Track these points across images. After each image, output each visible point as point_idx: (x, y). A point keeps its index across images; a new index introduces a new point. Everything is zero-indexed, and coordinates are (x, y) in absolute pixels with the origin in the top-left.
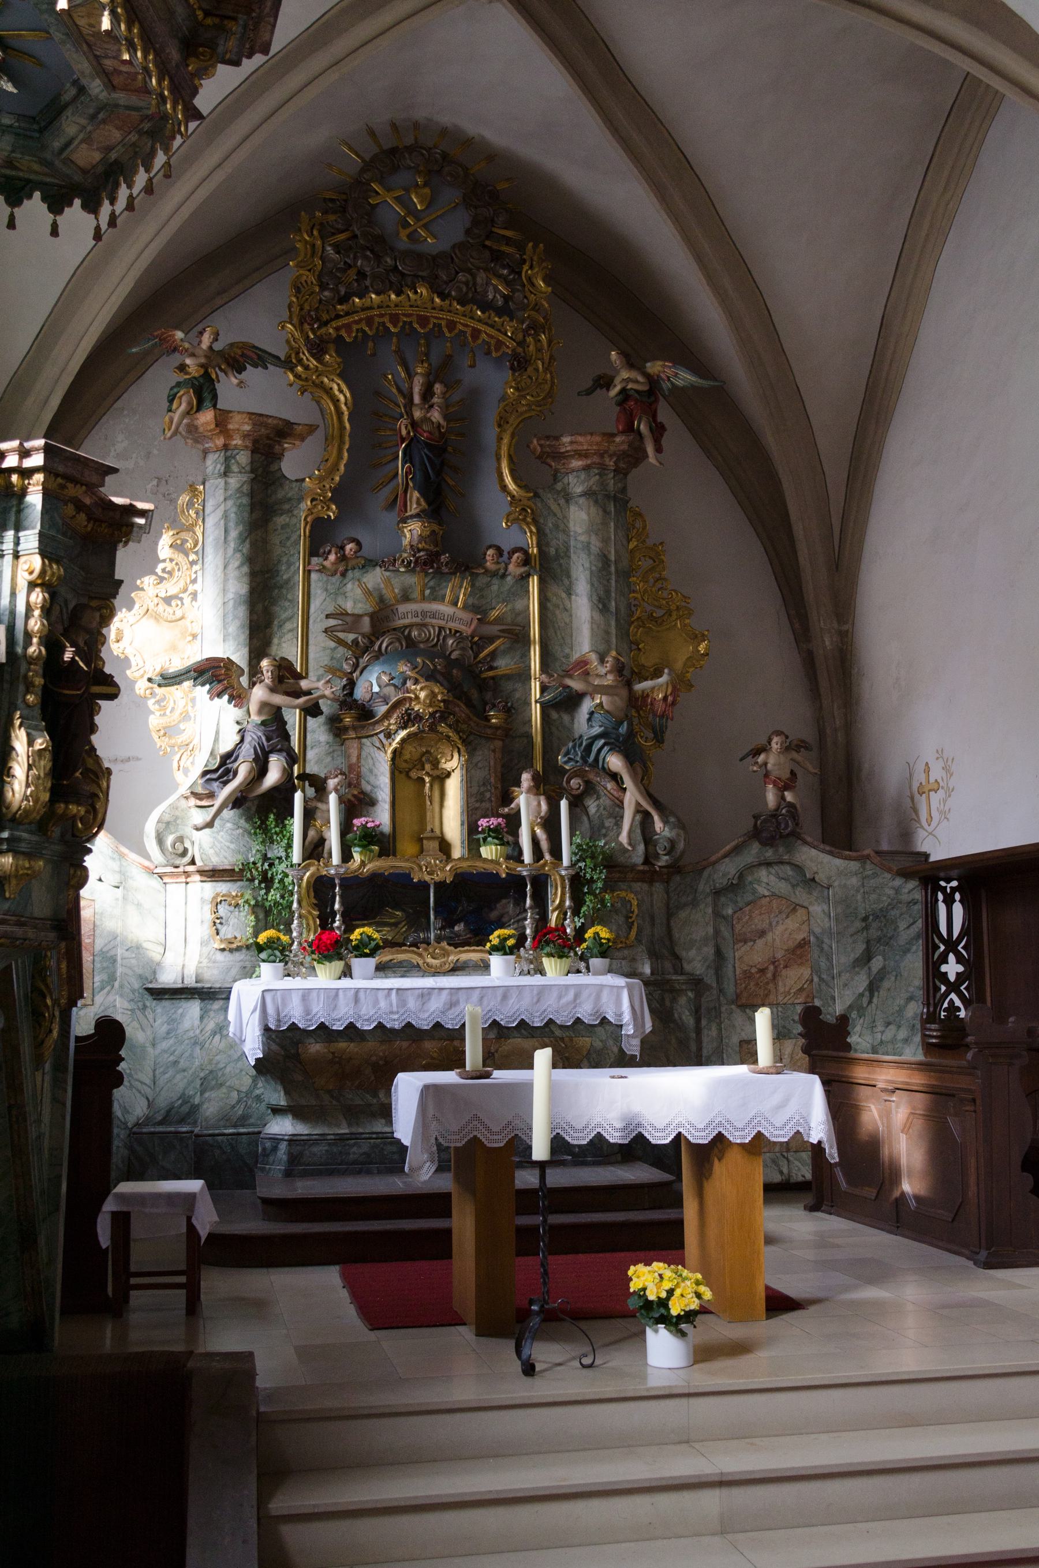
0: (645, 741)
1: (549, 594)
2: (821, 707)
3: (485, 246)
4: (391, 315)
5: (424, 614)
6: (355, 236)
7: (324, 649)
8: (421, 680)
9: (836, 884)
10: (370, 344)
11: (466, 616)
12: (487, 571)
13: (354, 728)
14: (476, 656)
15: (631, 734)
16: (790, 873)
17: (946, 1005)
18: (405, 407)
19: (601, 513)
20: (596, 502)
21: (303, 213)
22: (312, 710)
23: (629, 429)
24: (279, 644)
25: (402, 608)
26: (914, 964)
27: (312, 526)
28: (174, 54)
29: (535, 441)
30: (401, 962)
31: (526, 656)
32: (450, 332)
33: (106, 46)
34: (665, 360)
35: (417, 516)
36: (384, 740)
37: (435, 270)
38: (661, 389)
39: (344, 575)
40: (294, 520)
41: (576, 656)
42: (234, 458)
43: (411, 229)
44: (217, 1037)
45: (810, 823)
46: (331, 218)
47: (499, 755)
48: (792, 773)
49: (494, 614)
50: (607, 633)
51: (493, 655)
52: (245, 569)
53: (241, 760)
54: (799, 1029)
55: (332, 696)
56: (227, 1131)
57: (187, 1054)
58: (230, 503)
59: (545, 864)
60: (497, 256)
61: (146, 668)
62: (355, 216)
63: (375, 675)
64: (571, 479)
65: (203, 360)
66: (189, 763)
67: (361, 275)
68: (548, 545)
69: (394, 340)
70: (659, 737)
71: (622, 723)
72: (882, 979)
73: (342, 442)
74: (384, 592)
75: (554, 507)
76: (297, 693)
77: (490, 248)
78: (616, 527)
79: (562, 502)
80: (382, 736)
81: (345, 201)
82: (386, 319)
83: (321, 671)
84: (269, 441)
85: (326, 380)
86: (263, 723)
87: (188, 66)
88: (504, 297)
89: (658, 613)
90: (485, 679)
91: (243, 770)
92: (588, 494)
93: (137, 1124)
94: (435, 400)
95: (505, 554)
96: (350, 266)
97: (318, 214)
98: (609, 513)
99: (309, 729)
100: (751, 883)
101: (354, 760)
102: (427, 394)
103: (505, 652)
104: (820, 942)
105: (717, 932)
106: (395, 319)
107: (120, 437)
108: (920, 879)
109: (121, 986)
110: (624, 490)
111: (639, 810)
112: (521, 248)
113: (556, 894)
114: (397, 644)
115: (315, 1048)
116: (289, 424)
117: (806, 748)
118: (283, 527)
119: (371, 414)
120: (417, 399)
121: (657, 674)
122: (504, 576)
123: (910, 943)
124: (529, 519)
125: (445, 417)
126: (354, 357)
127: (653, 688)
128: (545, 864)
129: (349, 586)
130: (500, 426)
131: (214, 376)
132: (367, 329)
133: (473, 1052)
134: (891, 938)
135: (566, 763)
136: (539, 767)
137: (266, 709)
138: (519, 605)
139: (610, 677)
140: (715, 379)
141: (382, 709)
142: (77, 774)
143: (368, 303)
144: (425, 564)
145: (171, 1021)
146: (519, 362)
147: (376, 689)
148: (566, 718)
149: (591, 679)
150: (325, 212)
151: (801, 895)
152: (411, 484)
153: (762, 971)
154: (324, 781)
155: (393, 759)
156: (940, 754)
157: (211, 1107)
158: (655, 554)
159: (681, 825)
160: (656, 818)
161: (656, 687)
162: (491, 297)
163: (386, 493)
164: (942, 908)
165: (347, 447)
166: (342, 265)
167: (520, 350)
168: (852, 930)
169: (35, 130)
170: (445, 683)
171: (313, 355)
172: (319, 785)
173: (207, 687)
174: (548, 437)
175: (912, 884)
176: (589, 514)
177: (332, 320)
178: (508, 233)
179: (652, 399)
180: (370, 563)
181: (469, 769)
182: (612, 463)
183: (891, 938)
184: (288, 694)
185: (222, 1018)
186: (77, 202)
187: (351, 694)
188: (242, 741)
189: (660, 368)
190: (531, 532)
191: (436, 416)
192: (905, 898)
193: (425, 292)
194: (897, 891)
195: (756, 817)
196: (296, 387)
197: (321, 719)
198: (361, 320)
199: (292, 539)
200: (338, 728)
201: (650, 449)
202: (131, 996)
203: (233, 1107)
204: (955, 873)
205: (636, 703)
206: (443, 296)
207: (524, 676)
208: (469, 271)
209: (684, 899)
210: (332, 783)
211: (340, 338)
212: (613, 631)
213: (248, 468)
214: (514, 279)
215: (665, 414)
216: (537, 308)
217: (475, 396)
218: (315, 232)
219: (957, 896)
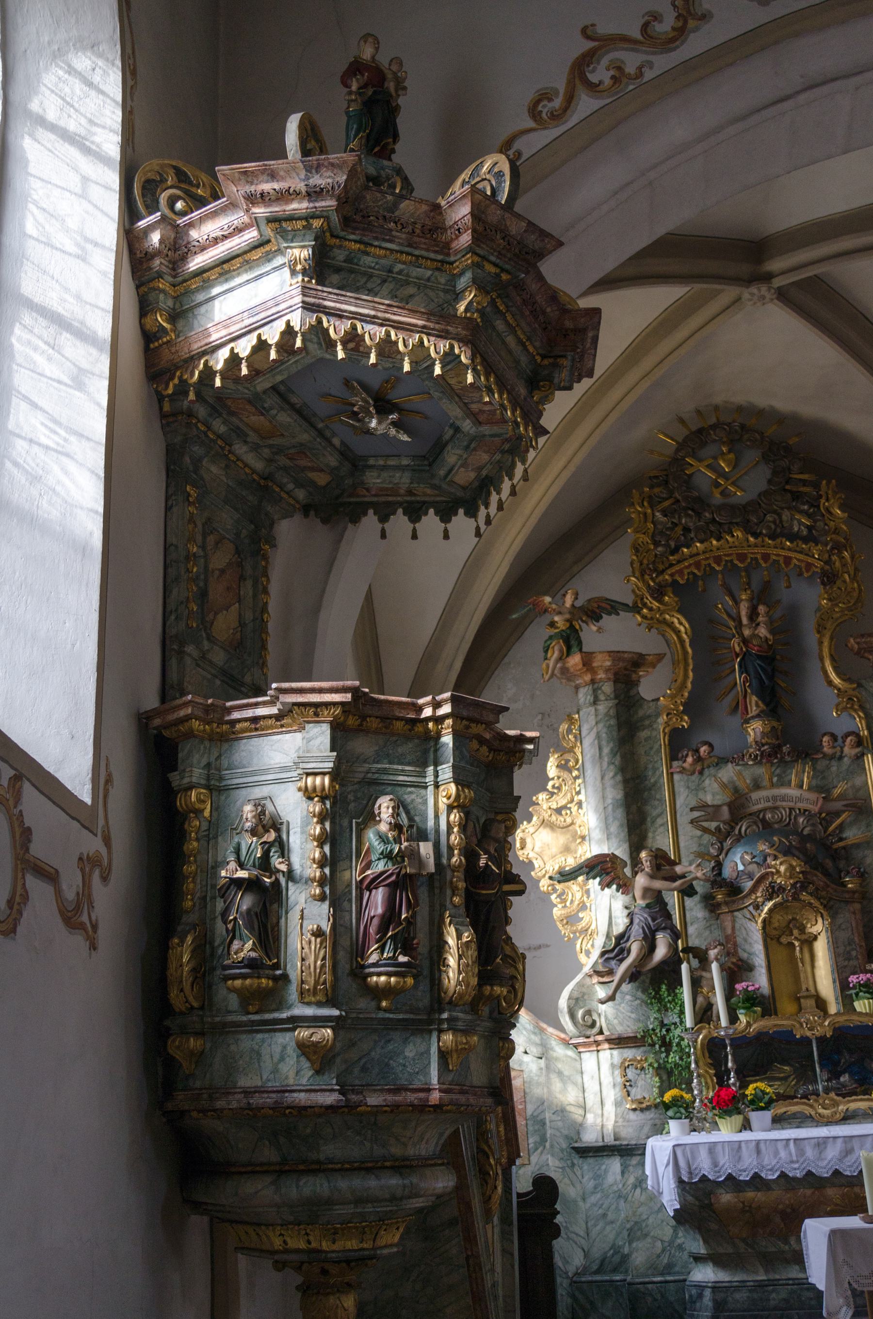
3: (785, 490)
4: (715, 557)
5: (775, 798)
6: (678, 501)
7: (692, 837)
10: (700, 583)
11: (813, 796)
12: (825, 755)
13: (727, 903)
22: (688, 891)
24: (654, 838)
25: (755, 796)
28: (522, 391)
29: (852, 640)
30: (794, 1114)
36: (754, 912)
37: (746, 516)
39: (701, 773)
42: (600, 689)
44: (638, 1191)
46: (656, 490)
51: (841, 827)
52: (619, 778)
53: (632, 939)
56: (655, 1279)
57: (613, 1207)
58: (601, 725)
60: (797, 496)
61: (547, 868)
63: (739, 855)
65: (568, 616)
66: (589, 946)
69: (720, 576)
74: (738, 783)
76: (673, 878)
77: (790, 491)
80: (751, 908)
82: (711, 561)
83: (692, 857)
84: (627, 672)
85: (667, 617)
86: (648, 906)
88: (807, 527)
94: (760, 619)
95: (840, 740)
96: (676, 525)
99: (687, 908)
101: (729, 931)
102: (753, 615)
109: (552, 1146)
112: (816, 486)
115: (726, 1198)
116: (641, 656)
118: (646, 739)
120: (745, 621)
122: (841, 758)
126: (689, 595)
129: (707, 782)
130: (819, 632)
131: (577, 627)
132: (696, 571)
141: (749, 884)
143: (694, 551)
144: (770, 755)
145: (596, 1177)
146: (828, 577)
147: (741, 867)
155: (764, 928)
157: (640, 1256)
162: (796, 529)
165: (691, 667)
166: (669, 525)
167: (827, 567)
171: (654, 599)
173: (598, 879)
174: (863, 636)
178: (805, 477)
180: (722, 761)
184: (665, 879)
186: (461, 511)
187: (720, 874)
190: (859, 717)
191: (763, 631)
193: (740, 534)
196: (644, 625)
197: (697, 898)
198: (690, 565)
200: (712, 905)
203: (659, 1256)
206: (756, 535)
208: (775, 512)
210: (712, 953)
216: (837, 531)
218: (646, 504)
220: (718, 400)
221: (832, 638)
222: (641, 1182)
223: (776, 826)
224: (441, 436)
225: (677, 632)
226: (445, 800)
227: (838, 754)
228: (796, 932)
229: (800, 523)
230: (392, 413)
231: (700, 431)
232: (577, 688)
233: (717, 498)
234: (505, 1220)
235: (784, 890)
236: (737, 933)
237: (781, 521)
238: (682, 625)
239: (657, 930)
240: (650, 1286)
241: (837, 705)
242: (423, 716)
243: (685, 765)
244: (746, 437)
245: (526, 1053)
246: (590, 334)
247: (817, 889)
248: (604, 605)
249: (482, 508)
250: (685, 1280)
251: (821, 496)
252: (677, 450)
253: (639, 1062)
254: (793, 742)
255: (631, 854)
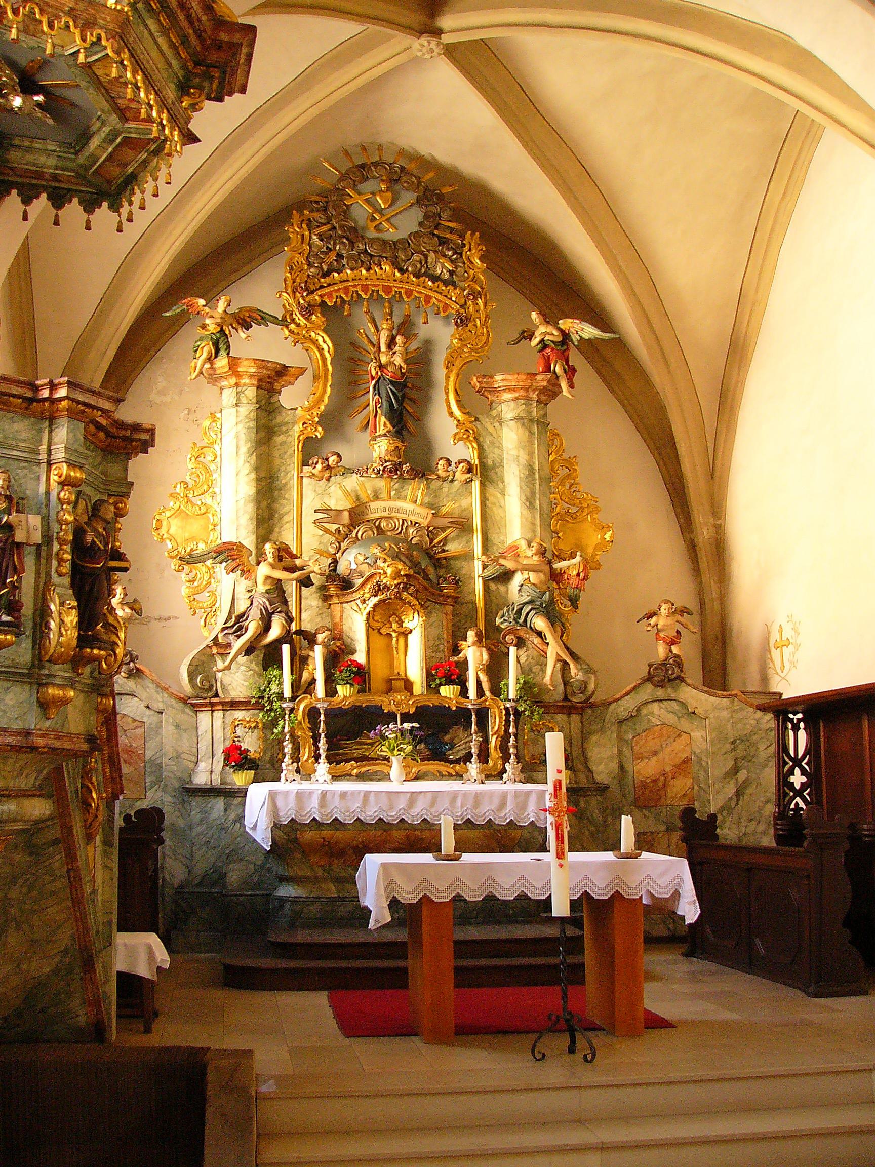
0: (564, 606)
1: (487, 495)
2: (701, 583)
3: (434, 235)
4: (362, 285)
5: (391, 509)
6: (334, 228)
7: (314, 536)
8: (389, 559)
9: (711, 716)
10: (347, 307)
11: (424, 511)
12: (439, 477)
13: (338, 596)
14: (432, 541)
15: (552, 601)
16: (677, 708)
17: (792, 806)
18: (374, 354)
19: (527, 433)
20: (523, 424)
21: (294, 212)
22: (306, 582)
23: (548, 369)
24: (279, 532)
25: (374, 505)
26: (770, 775)
27: (304, 444)
28: (171, 93)
29: (475, 379)
30: (376, 772)
31: (470, 541)
32: (408, 297)
33: (119, 89)
34: (574, 318)
35: (385, 435)
36: (360, 605)
37: (394, 252)
38: (572, 341)
39: (328, 480)
40: (290, 439)
41: (509, 542)
42: (243, 392)
43: (377, 222)
44: (238, 825)
45: (693, 670)
46: (316, 214)
47: (450, 617)
48: (678, 632)
49: (444, 510)
50: (533, 524)
51: (445, 541)
52: (253, 475)
53: (250, 619)
54: (680, 824)
55: (319, 572)
56: (247, 893)
57: (216, 836)
58: (241, 426)
59: (486, 700)
60: (443, 242)
61: (180, 550)
62: (334, 213)
63: (353, 555)
64: (504, 407)
65: (219, 320)
66: (212, 621)
67: (340, 256)
68: (486, 458)
69: (365, 303)
70: (574, 602)
71: (545, 593)
72: (746, 787)
73: (326, 380)
74: (359, 493)
75: (490, 428)
76: (292, 569)
77: (438, 236)
78: (539, 444)
79: (497, 425)
80: (358, 602)
81: (327, 202)
82: (359, 289)
83: (312, 552)
84: (272, 379)
85: (313, 334)
86: (267, 591)
87: (182, 102)
88: (449, 271)
89: (573, 510)
90: (439, 559)
91: (253, 627)
92: (518, 419)
93: (181, 886)
94: (397, 348)
95: (453, 465)
96: (330, 250)
97: (306, 212)
98: (533, 434)
99: (303, 596)
100: (646, 715)
101: (338, 620)
102: (391, 343)
103: (453, 539)
104: (700, 760)
105: (620, 752)
106: (365, 288)
107: (160, 379)
108: (774, 712)
109: (166, 786)
110: (545, 415)
111: (559, 659)
112: (462, 237)
113: (495, 722)
114: (370, 532)
115: (309, 836)
116: (285, 367)
117: (688, 614)
118: (281, 444)
119: (350, 360)
120: (383, 348)
121: (573, 556)
122: (452, 481)
123: (767, 760)
124: (471, 438)
125: (405, 361)
126: (335, 317)
127: (568, 567)
128: (486, 700)
129: (333, 488)
130: (447, 368)
131: (227, 332)
132: (344, 296)
133: (448, 842)
134: (753, 757)
135: (502, 623)
136: (482, 626)
137: (269, 581)
138: (464, 503)
139: (536, 558)
140: (614, 332)
141: (359, 582)
142: (99, 627)
143: (345, 278)
144: (391, 471)
145: (203, 812)
146: (461, 319)
147: (354, 566)
148: (502, 588)
149: (520, 560)
150: (312, 211)
151: (685, 725)
152: (379, 412)
153: (655, 781)
154: (315, 635)
155: (368, 619)
156: (790, 619)
157: (235, 875)
158: (569, 464)
159: (589, 670)
160: (572, 666)
161: (570, 566)
162: (439, 272)
163: (360, 418)
164: (791, 733)
165: (330, 383)
166: (324, 249)
167: (462, 311)
168: (724, 751)
169: (72, 154)
170: (408, 562)
171: (303, 316)
172: (310, 639)
173: (224, 564)
174: (484, 376)
175: (770, 716)
176: (517, 434)
177: (317, 290)
178: (450, 224)
179: (565, 347)
180: (347, 471)
181: (426, 627)
182: (535, 396)
183: (753, 757)
184: (286, 569)
185: (241, 810)
186: (105, 204)
187: (335, 570)
188: (251, 604)
189: (570, 325)
190: (473, 447)
191: (398, 360)
192: (764, 726)
193: (388, 268)
194: (758, 721)
195: (650, 665)
196: (291, 339)
197: (312, 589)
198: (339, 289)
199: (288, 454)
200: (325, 596)
201: (564, 385)
202: (174, 793)
203: (251, 876)
204: (800, 707)
205: (556, 576)
206: (402, 271)
207: (468, 556)
208: (422, 253)
209: (594, 727)
210: (320, 637)
211: (323, 302)
212: (538, 522)
213: (254, 400)
214: (457, 258)
215: (576, 358)
216: (474, 279)
217: (428, 346)
218: (304, 226)
219: (802, 725)
220: (384, 139)
221: (458, 375)
222: (241, 818)
223: (389, 534)
224: (89, 127)
225: (321, 350)
226: (56, 478)
227: (451, 477)
228: (395, 625)
229: (443, 266)
230: (37, 94)
231: (363, 166)
232: (221, 389)
233: (372, 234)
234: (107, 843)
235: (389, 589)
236: (344, 622)
237: (426, 262)
238: (326, 344)
239: (273, 613)
240: (242, 898)
241: (455, 435)
242: (57, 396)
243: (314, 471)
244: (404, 179)
245: (148, 707)
246: (244, 51)
247: (417, 591)
248: (254, 315)
249: (125, 204)
250: (271, 895)
251: (464, 245)
252: (339, 181)
253: (248, 722)
254: (414, 460)
255: (257, 544)
